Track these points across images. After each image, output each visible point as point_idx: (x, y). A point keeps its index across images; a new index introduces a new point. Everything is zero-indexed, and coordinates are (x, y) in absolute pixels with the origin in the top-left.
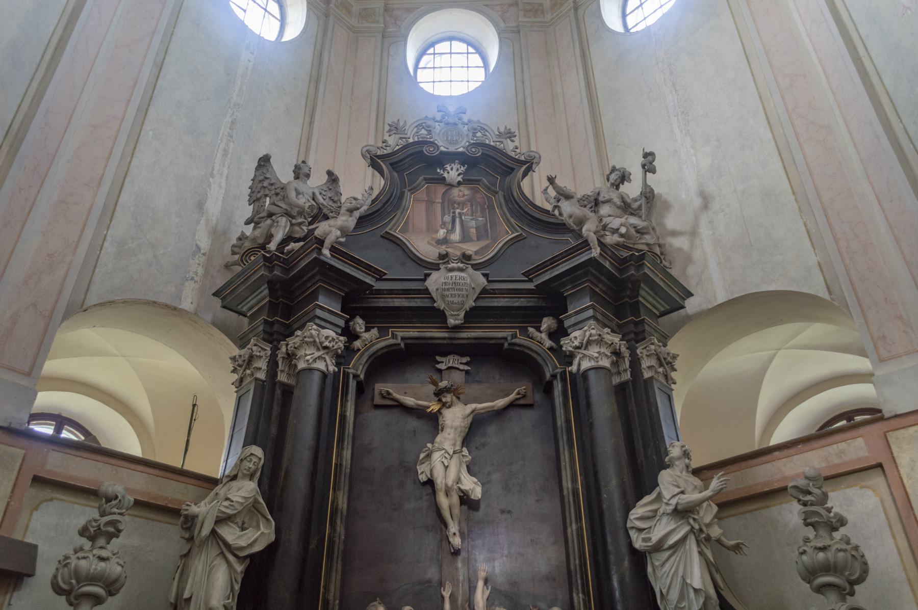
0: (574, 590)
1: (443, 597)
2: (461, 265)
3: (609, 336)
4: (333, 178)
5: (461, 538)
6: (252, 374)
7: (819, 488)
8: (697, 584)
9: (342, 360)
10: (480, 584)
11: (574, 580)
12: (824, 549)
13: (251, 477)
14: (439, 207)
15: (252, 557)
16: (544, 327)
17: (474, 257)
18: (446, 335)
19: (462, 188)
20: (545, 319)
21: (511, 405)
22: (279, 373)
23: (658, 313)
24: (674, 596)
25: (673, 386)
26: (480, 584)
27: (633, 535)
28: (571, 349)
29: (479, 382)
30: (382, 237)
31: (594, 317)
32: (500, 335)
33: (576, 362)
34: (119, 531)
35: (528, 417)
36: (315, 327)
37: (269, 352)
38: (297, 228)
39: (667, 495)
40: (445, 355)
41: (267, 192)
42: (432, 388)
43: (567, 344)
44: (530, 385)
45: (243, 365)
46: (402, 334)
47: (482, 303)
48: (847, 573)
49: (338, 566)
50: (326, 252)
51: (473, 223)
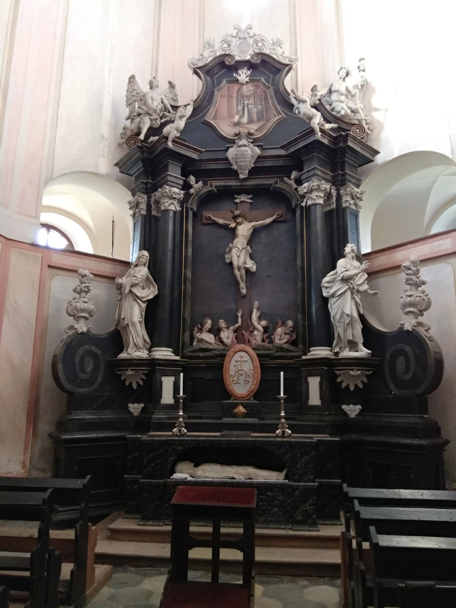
1: (237, 316)
4: (172, 85)
6: (140, 212)
7: (416, 267)
8: (348, 312)
12: (410, 296)
13: (144, 265)
15: (149, 301)
16: (292, 177)
19: (249, 85)
21: (274, 222)
23: (357, 166)
24: (338, 317)
25: (360, 210)
26: (255, 310)
27: (324, 290)
29: (258, 209)
30: (203, 123)
33: (305, 200)
34: (90, 290)
35: (283, 227)
37: (146, 200)
39: (339, 273)
40: (239, 194)
41: (136, 99)
42: (232, 215)
45: (135, 206)
47: (259, 165)
48: (419, 307)
49: (189, 303)
50: (170, 144)
51: (255, 110)
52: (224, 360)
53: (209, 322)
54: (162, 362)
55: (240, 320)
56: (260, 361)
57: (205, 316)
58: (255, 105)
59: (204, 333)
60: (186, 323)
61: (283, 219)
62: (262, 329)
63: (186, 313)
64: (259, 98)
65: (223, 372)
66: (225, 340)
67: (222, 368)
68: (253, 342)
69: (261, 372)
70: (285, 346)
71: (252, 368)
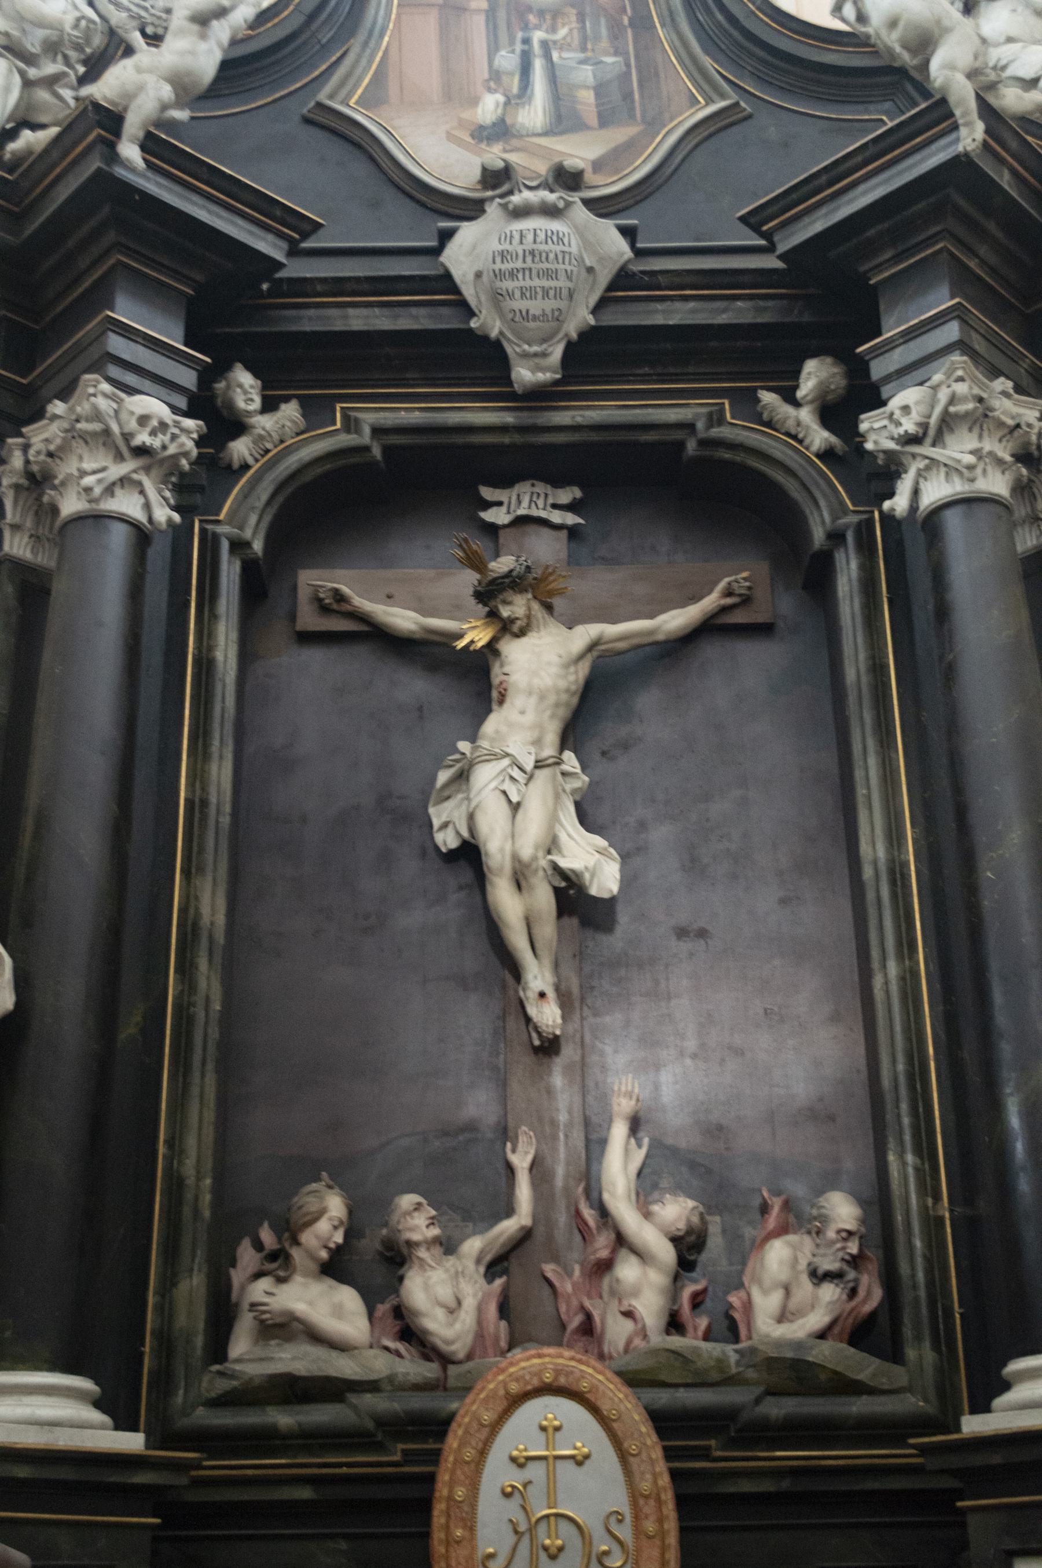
0: (892, 1144)
1: (510, 1169)
2: (551, 197)
3: (1007, 404)
5: (562, 1006)
9: (198, 499)
10: (619, 1131)
11: (889, 1117)
14: (479, 23)
17: (589, 177)
18: (509, 418)
20: (811, 366)
22: (7, 534)
26: (619, 1131)
28: (891, 445)
30: (307, 121)
31: (961, 346)
32: (672, 415)
35: (755, 663)
36: (105, 387)
38: (43, 95)
40: (506, 482)
42: (470, 578)
43: (877, 431)
44: (763, 568)
46: (372, 417)
49: (205, 1084)
50: (130, 151)
51: (586, 74)
52: (435, 1457)
53: (335, 1205)
54: (22, 1472)
55: (524, 1192)
56: (670, 1454)
57: (309, 1169)
58: (584, 49)
59: (298, 1279)
60: (187, 1211)
61: (760, 617)
62: (667, 1253)
63: (191, 1142)
64: (603, 21)
65: (426, 1536)
66: (436, 1324)
67: (424, 1506)
68: (617, 1331)
69: (683, 1530)
70: (827, 1353)
71: (626, 1510)
